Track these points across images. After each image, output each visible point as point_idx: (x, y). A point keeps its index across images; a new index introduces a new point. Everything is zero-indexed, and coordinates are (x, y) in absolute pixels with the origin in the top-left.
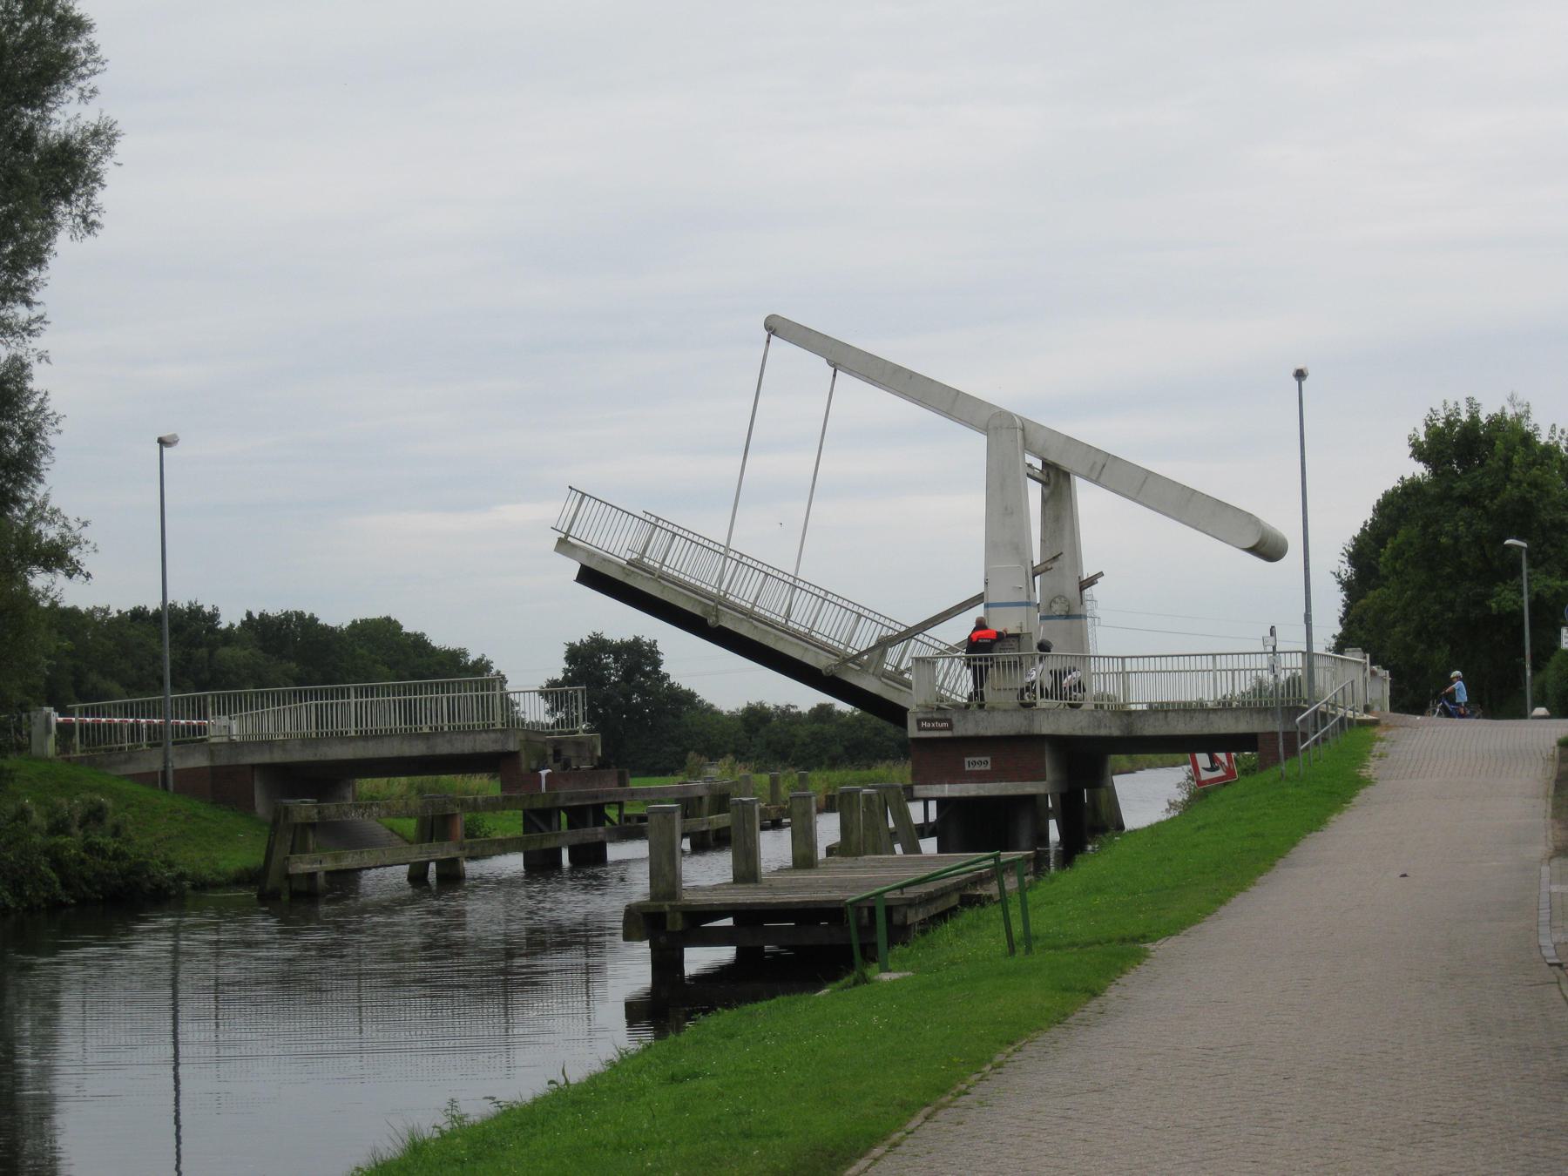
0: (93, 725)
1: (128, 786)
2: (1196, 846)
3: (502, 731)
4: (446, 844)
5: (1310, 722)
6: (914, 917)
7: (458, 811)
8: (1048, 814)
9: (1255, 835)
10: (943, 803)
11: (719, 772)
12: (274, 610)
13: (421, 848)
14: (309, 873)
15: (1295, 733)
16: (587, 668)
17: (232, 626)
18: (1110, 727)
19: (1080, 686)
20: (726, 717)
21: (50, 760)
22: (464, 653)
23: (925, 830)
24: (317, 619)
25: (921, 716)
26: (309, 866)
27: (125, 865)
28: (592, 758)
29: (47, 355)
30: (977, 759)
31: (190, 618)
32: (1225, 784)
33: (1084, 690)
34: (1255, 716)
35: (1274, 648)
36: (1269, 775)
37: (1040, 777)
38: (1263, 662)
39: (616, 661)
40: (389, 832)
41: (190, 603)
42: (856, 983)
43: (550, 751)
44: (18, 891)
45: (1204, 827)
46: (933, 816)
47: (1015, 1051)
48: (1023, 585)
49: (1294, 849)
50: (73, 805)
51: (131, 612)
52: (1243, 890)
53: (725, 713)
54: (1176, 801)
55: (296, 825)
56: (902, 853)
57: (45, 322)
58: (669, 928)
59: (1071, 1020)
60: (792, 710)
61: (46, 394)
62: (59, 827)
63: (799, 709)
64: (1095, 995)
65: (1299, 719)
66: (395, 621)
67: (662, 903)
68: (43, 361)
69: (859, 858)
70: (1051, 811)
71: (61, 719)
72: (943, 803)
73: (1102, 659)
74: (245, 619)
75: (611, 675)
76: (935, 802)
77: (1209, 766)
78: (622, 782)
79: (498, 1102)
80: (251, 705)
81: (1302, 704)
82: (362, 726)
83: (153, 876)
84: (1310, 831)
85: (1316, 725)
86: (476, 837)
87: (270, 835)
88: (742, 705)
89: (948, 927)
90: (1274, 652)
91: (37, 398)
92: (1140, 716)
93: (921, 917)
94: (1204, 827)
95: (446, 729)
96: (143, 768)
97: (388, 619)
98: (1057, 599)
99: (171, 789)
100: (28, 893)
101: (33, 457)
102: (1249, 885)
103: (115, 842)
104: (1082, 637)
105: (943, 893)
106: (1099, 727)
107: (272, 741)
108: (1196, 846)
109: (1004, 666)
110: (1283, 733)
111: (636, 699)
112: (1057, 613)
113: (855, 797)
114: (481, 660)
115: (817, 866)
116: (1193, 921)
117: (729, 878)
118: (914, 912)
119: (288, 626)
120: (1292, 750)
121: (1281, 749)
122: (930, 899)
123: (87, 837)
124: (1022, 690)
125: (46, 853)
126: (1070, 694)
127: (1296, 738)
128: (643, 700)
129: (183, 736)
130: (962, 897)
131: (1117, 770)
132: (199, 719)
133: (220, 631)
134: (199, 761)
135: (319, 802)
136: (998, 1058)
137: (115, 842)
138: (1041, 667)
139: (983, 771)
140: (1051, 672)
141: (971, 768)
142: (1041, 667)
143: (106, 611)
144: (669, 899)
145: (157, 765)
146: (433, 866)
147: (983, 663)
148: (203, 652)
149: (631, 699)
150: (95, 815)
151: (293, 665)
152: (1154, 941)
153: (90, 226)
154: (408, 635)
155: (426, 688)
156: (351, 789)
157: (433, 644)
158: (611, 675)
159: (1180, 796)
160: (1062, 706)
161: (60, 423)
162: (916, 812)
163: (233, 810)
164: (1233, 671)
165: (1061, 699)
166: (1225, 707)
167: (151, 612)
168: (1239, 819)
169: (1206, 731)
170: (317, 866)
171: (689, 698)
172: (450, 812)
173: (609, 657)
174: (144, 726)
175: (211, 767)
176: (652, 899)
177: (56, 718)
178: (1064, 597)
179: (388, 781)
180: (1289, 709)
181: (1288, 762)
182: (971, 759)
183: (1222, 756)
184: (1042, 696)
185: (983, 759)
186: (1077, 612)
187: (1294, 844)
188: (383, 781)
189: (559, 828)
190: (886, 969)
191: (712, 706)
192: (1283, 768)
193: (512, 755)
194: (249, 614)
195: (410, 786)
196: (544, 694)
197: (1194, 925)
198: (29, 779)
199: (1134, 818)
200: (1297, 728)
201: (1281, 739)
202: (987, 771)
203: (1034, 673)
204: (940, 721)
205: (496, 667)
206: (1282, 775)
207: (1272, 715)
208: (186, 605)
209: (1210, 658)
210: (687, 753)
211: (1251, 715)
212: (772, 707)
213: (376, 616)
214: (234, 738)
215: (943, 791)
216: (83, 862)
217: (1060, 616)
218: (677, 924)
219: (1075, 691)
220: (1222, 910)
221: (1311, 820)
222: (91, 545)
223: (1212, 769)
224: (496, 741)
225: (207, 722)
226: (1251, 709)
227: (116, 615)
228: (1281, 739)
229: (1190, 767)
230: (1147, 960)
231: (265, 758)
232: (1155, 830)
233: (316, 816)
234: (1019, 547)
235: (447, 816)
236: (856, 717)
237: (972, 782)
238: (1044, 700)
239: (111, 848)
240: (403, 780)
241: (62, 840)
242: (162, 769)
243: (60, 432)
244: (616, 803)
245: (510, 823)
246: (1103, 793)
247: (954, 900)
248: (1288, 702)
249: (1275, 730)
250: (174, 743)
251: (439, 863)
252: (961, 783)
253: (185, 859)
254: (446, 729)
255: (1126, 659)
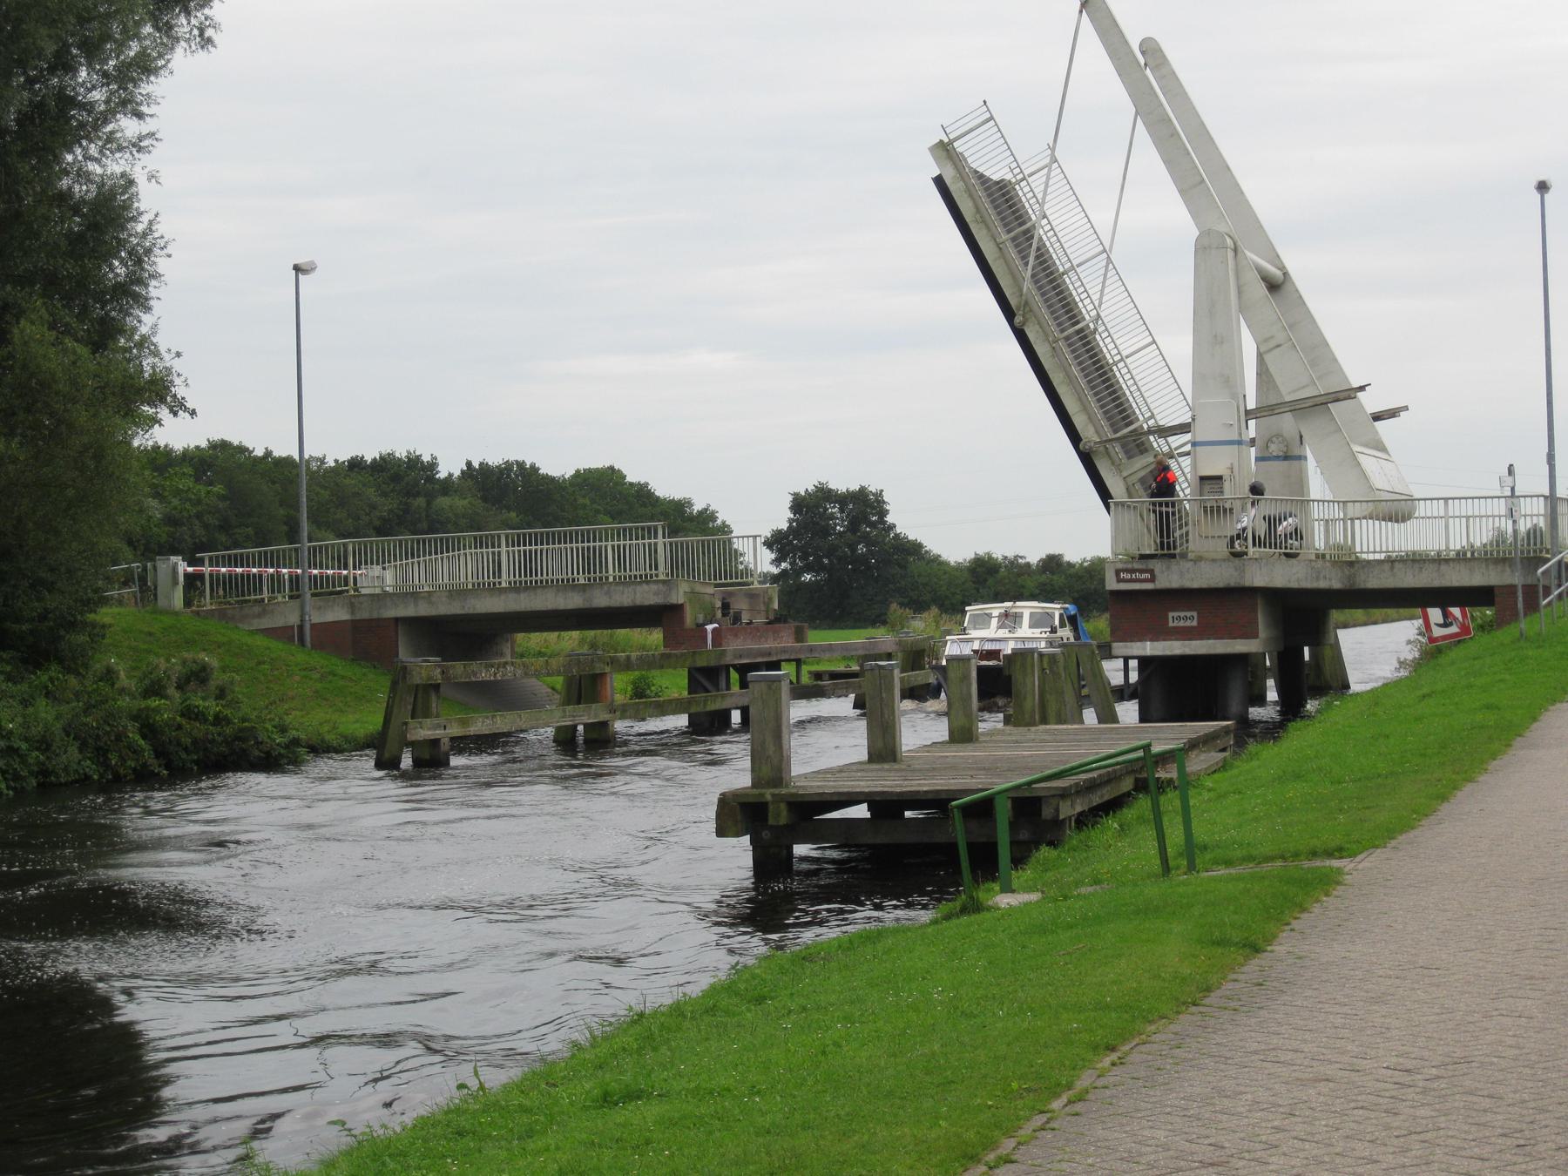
0: (242, 575)
1: (261, 641)
2: (1419, 719)
3: (664, 582)
4: (594, 706)
5: (1554, 573)
6: (1068, 810)
7: (607, 669)
8: (1265, 673)
9: (1488, 707)
10: (1145, 662)
11: (924, 625)
12: (495, 460)
13: (564, 711)
14: (431, 740)
15: (1536, 586)
16: (812, 517)
17: (450, 475)
18: (1330, 579)
19: (1297, 534)
20: (953, 567)
21: (176, 614)
22: (689, 503)
23: (1123, 693)
24: (539, 469)
25: (1120, 566)
26: (430, 733)
27: (228, 731)
28: (767, 611)
29: (158, 175)
30: (1182, 614)
31: (408, 468)
32: (1459, 641)
33: (1302, 538)
34: (1491, 567)
35: (1513, 489)
36: (1506, 634)
37: (1253, 635)
38: (1501, 507)
39: (842, 510)
40: (550, 690)
41: (409, 452)
42: (964, 910)
43: (719, 604)
44: (101, 759)
45: (1429, 695)
46: (1134, 677)
47: (1113, 1064)
48: (1234, 421)
49: (1535, 725)
50: (170, 665)
51: (348, 461)
52: (1471, 780)
53: (952, 563)
54: (1406, 659)
55: (417, 686)
56: (1096, 721)
57: (157, 139)
58: (771, 822)
59: (1213, 999)
60: (1020, 561)
61: (156, 215)
62: (154, 689)
63: (1028, 560)
64: (1256, 950)
65: (1540, 571)
66: (619, 470)
67: (763, 791)
68: (153, 180)
69: (1033, 729)
70: (1270, 669)
71: (190, 569)
72: (1145, 662)
73: (1316, 503)
74: (465, 468)
75: (836, 525)
76: (1136, 661)
77: (1442, 621)
78: (799, 636)
79: (350, 1130)
80: (395, 556)
81: (1544, 555)
82: (542, 575)
83: (262, 743)
84: (1554, 702)
85: (1559, 577)
86: (646, 697)
87: (389, 697)
88: (970, 556)
89: (1112, 823)
90: (1513, 495)
91: (145, 219)
92: (1363, 567)
93: (1079, 809)
94: (1429, 695)
95: (611, 579)
96: (278, 622)
97: (612, 468)
98: (1274, 439)
99: (309, 645)
100: (113, 762)
101: (140, 282)
102: (1479, 773)
103: (217, 705)
104: (1301, 480)
105: (1110, 779)
106: (1318, 579)
107: (417, 593)
108: (1419, 719)
109: (1212, 511)
110: (1523, 586)
111: (862, 549)
112: (1274, 454)
113: (1029, 658)
114: (706, 510)
115: (977, 740)
116: (1404, 826)
117: (865, 757)
118: (1070, 803)
119: (509, 476)
120: (1532, 606)
121: (1520, 605)
122: (1091, 787)
123: (186, 700)
124: (1232, 538)
125: (135, 718)
126: (1286, 542)
127: (1537, 592)
128: (868, 550)
129: (322, 587)
130: (1137, 780)
131: (1352, 624)
132: (260, 566)
133: (439, 480)
134: (337, 613)
135: (443, 661)
136: (1085, 1080)
137: (217, 705)
138: (1253, 512)
139: (1189, 627)
140: (1264, 518)
141: (1176, 624)
142: (1253, 512)
143: (322, 461)
144: (775, 786)
145: (293, 619)
146: (580, 728)
147: (1170, 510)
148: (420, 502)
149: (856, 549)
150: (197, 676)
151: (513, 514)
152: (1353, 855)
153: (206, 42)
154: (631, 484)
155: (583, 536)
156: (509, 645)
157: (657, 493)
158: (836, 525)
159: (1411, 654)
160: (1277, 554)
161: (169, 247)
162: (1113, 671)
163: (375, 667)
164: (1468, 518)
165: (1276, 548)
166: (1461, 558)
167: (370, 460)
168: (1470, 686)
169: (1437, 583)
170: (438, 733)
171: (915, 548)
172: (598, 672)
173: (834, 507)
174: (286, 577)
175: (352, 621)
176: (754, 785)
177: (183, 567)
178: (1282, 436)
179: (559, 636)
180: (1529, 559)
181: (1528, 618)
182: (1176, 614)
183: (1456, 611)
184: (1254, 545)
185: (1188, 614)
186: (1297, 452)
187: (1535, 719)
188: (553, 636)
189: (728, 688)
190: (1008, 889)
191: (939, 556)
192: (1523, 626)
193: (677, 609)
194: (469, 464)
195: (582, 641)
196: (769, 544)
197: (1406, 831)
198: (150, 634)
199: (1360, 678)
200: (1539, 580)
201: (1520, 594)
202: (1192, 627)
203: (1246, 519)
204: (1141, 571)
205: (721, 517)
206: (1522, 635)
207: (1510, 566)
208: (404, 455)
209: (1442, 502)
210: (888, 606)
211: (1487, 566)
212: (1000, 557)
213: (600, 466)
214: (388, 589)
215: (1145, 649)
216: (180, 727)
217: (1277, 458)
218: (780, 816)
219: (1291, 539)
220: (1445, 808)
221: (1555, 688)
222: (182, 379)
223: (1445, 625)
224: (656, 594)
225: (299, 571)
226: (1487, 560)
227: (333, 464)
228: (1520, 594)
229: (1421, 621)
230: (1338, 887)
231: (409, 611)
232: (1389, 687)
233: (439, 677)
234: (1230, 382)
235: (597, 675)
236: (1086, 568)
237: (1177, 640)
238: (1257, 549)
239: (212, 713)
240: (575, 634)
241: (154, 702)
242: (299, 623)
243: (169, 256)
244: (793, 660)
245: (674, 683)
246: (1327, 652)
247: (1127, 784)
248: (1529, 552)
249: (1514, 583)
250: (313, 595)
251: (585, 725)
252: (1164, 640)
253: (301, 724)
254: (611, 579)
255: (1349, 504)
